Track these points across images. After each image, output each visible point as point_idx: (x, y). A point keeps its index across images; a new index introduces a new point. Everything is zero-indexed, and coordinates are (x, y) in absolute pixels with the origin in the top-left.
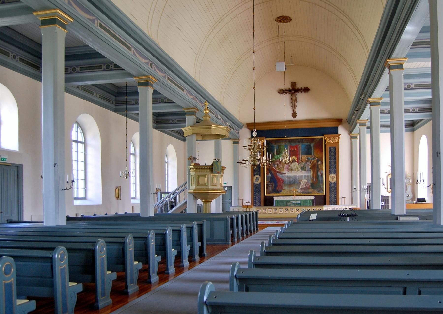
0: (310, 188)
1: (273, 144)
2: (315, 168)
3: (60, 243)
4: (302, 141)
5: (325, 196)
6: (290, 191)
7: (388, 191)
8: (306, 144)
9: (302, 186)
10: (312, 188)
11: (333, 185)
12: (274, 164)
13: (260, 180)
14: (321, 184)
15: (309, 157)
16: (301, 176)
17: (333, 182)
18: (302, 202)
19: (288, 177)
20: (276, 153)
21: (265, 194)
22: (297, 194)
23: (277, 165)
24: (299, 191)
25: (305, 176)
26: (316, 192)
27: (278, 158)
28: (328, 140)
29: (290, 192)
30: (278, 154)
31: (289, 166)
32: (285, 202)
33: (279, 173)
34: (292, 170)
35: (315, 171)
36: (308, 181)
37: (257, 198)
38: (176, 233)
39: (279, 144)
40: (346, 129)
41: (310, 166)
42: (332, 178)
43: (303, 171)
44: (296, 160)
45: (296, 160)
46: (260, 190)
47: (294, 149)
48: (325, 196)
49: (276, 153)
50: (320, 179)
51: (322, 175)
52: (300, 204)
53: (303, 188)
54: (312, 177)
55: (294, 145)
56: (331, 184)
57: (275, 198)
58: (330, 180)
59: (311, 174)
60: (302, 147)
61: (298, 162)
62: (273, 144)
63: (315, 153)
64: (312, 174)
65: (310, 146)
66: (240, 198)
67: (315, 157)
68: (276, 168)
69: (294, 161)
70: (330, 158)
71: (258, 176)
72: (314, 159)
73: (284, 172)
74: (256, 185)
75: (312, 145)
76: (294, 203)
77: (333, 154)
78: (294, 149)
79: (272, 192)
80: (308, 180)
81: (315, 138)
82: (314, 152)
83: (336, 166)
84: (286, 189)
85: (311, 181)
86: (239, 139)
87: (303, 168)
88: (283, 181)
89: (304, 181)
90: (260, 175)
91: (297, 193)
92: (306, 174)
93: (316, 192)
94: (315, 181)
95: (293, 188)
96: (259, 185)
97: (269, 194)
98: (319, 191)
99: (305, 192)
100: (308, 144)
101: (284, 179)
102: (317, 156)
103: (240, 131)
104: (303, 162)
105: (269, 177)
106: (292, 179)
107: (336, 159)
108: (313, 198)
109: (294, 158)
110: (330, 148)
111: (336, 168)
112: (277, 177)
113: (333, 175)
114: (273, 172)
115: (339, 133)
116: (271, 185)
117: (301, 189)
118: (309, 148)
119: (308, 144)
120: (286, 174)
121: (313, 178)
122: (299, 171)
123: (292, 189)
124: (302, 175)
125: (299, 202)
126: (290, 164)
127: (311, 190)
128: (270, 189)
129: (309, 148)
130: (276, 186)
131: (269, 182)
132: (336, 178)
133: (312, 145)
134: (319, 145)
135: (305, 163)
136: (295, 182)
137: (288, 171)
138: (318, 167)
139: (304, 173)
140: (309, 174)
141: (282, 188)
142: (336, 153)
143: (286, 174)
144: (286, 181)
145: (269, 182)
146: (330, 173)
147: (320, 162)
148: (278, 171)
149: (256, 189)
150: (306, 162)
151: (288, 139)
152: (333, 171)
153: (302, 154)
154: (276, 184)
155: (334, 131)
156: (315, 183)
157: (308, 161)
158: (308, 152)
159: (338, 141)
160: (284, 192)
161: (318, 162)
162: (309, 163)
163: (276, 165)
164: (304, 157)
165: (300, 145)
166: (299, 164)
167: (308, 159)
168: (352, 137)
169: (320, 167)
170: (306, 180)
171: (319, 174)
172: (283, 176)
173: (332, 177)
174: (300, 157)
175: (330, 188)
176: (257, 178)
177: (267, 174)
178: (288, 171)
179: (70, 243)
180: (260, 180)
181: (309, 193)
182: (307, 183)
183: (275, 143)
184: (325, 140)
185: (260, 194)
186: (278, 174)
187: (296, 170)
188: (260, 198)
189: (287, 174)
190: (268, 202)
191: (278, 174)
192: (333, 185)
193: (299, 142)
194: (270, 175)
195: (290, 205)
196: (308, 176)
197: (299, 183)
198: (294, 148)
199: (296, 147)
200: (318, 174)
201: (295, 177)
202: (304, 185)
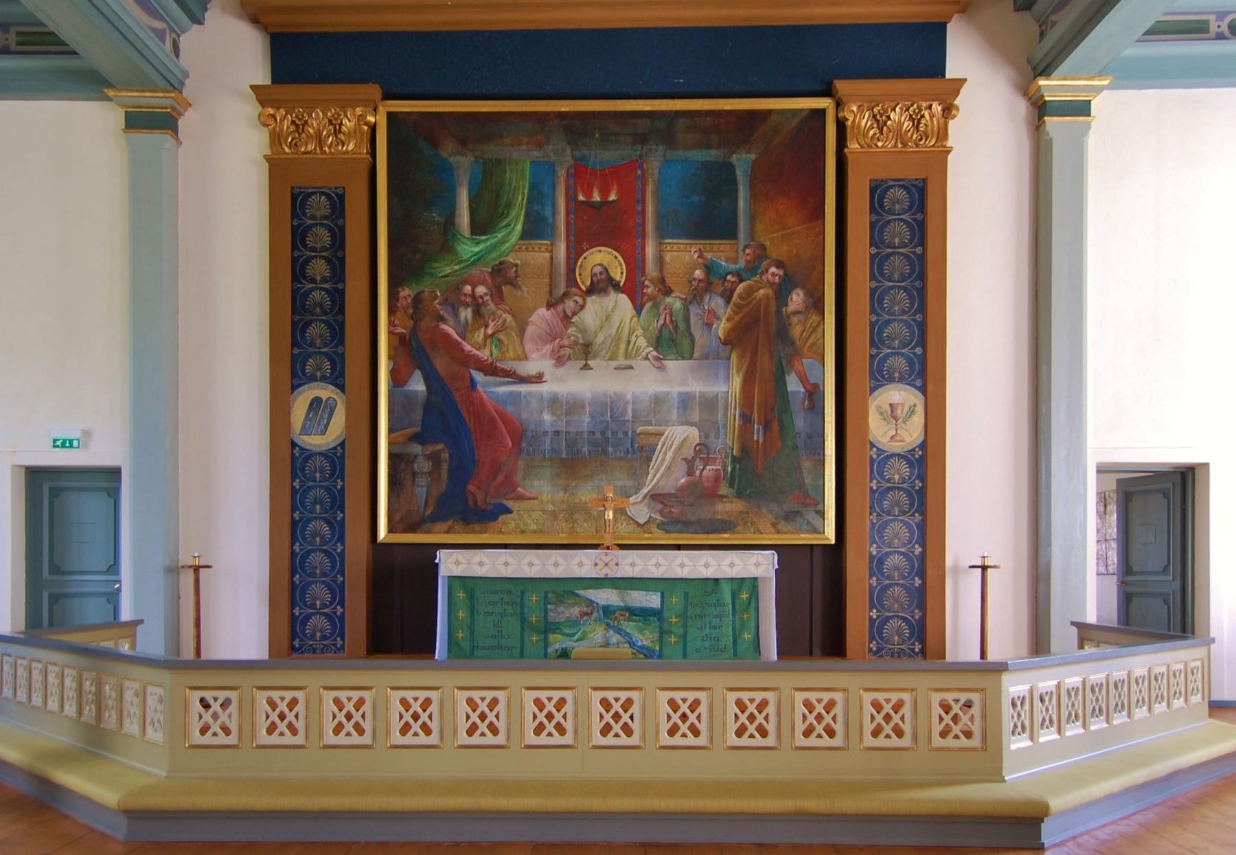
0: (724, 490)
1: (448, 150)
2: (761, 341)
4: (664, 129)
5: (835, 554)
6: (573, 511)
8: (698, 155)
9: (664, 471)
10: (739, 495)
11: (898, 472)
14: (806, 465)
15: (721, 254)
16: (658, 401)
17: (897, 447)
18: (675, 600)
19: (554, 401)
21: (382, 533)
22: (625, 531)
23: (477, 313)
24: (641, 511)
25: (686, 401)
26: (765, 522)
27: (478, 259)
28: (865, 121)
29: (570, 519)
30: (480, 227)
31: (567, 319)
32: (533, 598)
33: (491, 370)
34: (585, 351)
35: (764, 360)
36: (705, 434)
37: (318, 560)
38: (1155, 511)
39: (492, 151)
40: (997, 46)
41: (721, 328)
42: (890, 416)
43: (671, 364)
44: (619, 273)
45: (619, 273)
46: (338, 501)
47: (605, 192)
48: (835, 554)
50: (800, 422)
51: (814, 394)
52: (656, 614)
53: (669, 486)
54: (735, 411)
55: (603, 156)
56: (883, 459)
57: (451, 564)
58: (879, 430)
60: (661, 175)
61: (632, 289)
62: (448, 150)
63: (764, 227)
64: (737, 382)
65: (727, 171)
66: (185, 559)
67: (761, 253)
69: (602, 285)
70: (878, 263)
71: (325, 391)
72: (753, 269)
74: (308, 455)
75: (743, 161)
76: (608, 611)
78: (605, 192)
79: (436, 518)
80: (708, 428)
81: (768, 113)
82: (752, 217)
83: (923, 327)
84: (543, 489)
85: (727, 441)
86: (175, 85)
87: (670, 342)
88: (518, 433)
89: (679, 435)
91: (623, 528)
92: (696, 387)
93: (765, 522)
94: (758, 435)
96: (336, 458)
97: (412, 528)
98: (789, 517)
99: (687, 517)
100: (713, 155)
102: (779, 250)
103: (192, 38)
104: (668, 292)
105: (410, 397)
107: (922, 276)
109: (601, 258)
110: (878, 190)
111: (923, 342)
112: (479, 409)
113: (899, 395)
114: (440, 363)
115: (951, 72)
116: (424, 465)
117: (655, 497)
118: (719, 182)
119: (713, 155)
120: (538, 379)
121: (746, 419)
122: (639, 363)
123: (585, 494)
124: (663, 389)
126: (570, 305)
127: (728, 507)
128: (421, 492)
130: (461, 472)
132: (918, 419)
133: (743, 161)
134: (798, 165)
135: (687, 303)
136: (610, 443)
137: (560, 361)
138: (783, 333)
139: (679, 379)
140: (719, 388)
141: (510, 487)
142: (922, 225)
143: (538, 379)
146: (880, 378)
147: (797, 298)
148: (484, 354)
149: (308, 489)
150: (696, 295)
151: (562, 115)
152: (900, 363)
153: (662, 234)
154: (465, 455)
155: (914, 54)
156: (757, 466)
157: (706, 286)
158: (709, 219)
159: (943, 134)
160: (524, 518)
162: (717, 303)
163: (466, 314)
164: (681, 257)
165: (654, 164)
166: (638, 309)
167: (709, 268)
168: (1040, 109)
169: (796, 331)
170: (693, 434)
171: (793, 384)
172: (516, 398)
174: (650, 250)
176: (316, 402)
177: (397, 379)
178: (560, 361)
179: (349, 684)
181: (725, 526)
182: (703, 451)
183: (463, 143)
184: (841, 125)
186: (478, 376)
187: (621, 354)
188: (338, 562)
189: (549, 384)
190: (397, 616)
191: (478, 376)
193: (641, 139)
194: (417, 385)
195: (574, 623)
196: (709, 403)
198: (607, 177)
199: (626, 176)
202: (681, 468)
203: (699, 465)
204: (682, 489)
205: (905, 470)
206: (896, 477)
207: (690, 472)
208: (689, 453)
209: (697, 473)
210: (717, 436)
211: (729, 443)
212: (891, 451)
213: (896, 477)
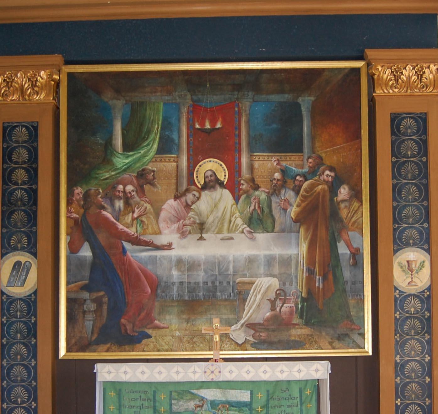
0: (296, 320)
1: (108, 96)
2: (321, 220)
3: (107, 408)
7: (277, 291)
8: (276, 98)
9: (256, 308)
10: (307, 323)
12: (111, 197)
13: (33, 277)
14: (352, 302)
15: (293, 163)
16: (251, 261)
17: (413, 290)
18: (261, 397)
19: (180, 262)
20: (118, 141)
21: (63, 352)
23: (127, 203)
24: (239, 334)
25: (270, 261)
31: (188, 207)
32: (162, 396)
33: (136, 241)
35: (322, 233)
39: (138, 97)
41: (293, 211)
44: (223, 175)
45: (223, 175)
46: (32, 331)
47: (213, 123)
48: (372, 363)
49: (118, 141)
50: (347, 274)
51: (356, 255)
54: (303, 267)
55: (212, 100)
56: (401, 299)
57: (105, 373)
58: (400, 279)
59: (297, 249)
61: (233, 186)
62: (108, 96)
63: (324, 148)
64: (304, 248)
65: (298, 106)
67: (320, 162)
68: (118, 216)
69: (212, 183)
70: (397, 169)
71: (23, 257)
72: (313, 172)
73: (162, 240)
75: (306, 102)
77: (410, 147)
78: (213, 123)
80: (284, 280)
82: (313, 138)
85: (298, 287)
87: (259, 221)
89: (265, 284)
90: (32, 250)
92: (277, 251)
94: (319, 284)
95: (213, 325)
96: (31, 302)
97: (83, 349)
100: (286, 97)
101: (160, 272)
102: (332, 159)
105: (81, 262)
106: (200, 276)
108: (321, 371)
112: (128, 268)
114: (102, 237)
118: (289, 117)
119: (286, 97)
120: (169, 247)
121: (311, 272)
122: (237, 236)
125: (245, 396)
126: (190, 197)
128: (88, 324)
129: (289, 117)
130: (116, 311)
131: (85, 288)
133: (306, 102)
134: (343, 102)
136: (213, 294)
137: (183, 235)
138: (334, 214)
139: (264, 246)
140: (292, 251)
141: (149, 320)
143: (169, 247)
144: (168, 286)
145: (85, 288)
146: (400, 243)
147: (344, 192)
148: (132, 231)
150: (275, 191)
152: (413, 233)
153: (251, 150)
157: (283, 183)
158: (284, 140)
161: (333, 188)
162: (289, 194)
163: (119, 204)
164: (267, 164)
166: (237, 199)
167: (284, 172)
169: (344, 213)
170: (275, 283)
171: (343, 249)
172: (153, 260)
173: (409, 267)
174: (244, 160)
175: (399, 323)
176: (18, 264)
177: (73, 248)
178: (183, 235)
180: (33, 277)
182: (281, 295)
183: (118, 91)
185: (33, 351)
186: (127, 245)
188: (32, 373)
191: (127, 245)
192: (413, 306)
193: (238, 87)
194: (86, 252)
196: (286, 262)
197: (240, 296)
199: (228, 112)
200: (333, 248)
201: (217, 266)
203: (279, 303)
204: (268, 320)
205: (419, 305)
206: (412, 310)
207: (273, 308)
208: (272, 296)
209: (278, 309)
210: (291, 284)
211: (299, 288)
212: (408, 292)
213: (412, 310)
